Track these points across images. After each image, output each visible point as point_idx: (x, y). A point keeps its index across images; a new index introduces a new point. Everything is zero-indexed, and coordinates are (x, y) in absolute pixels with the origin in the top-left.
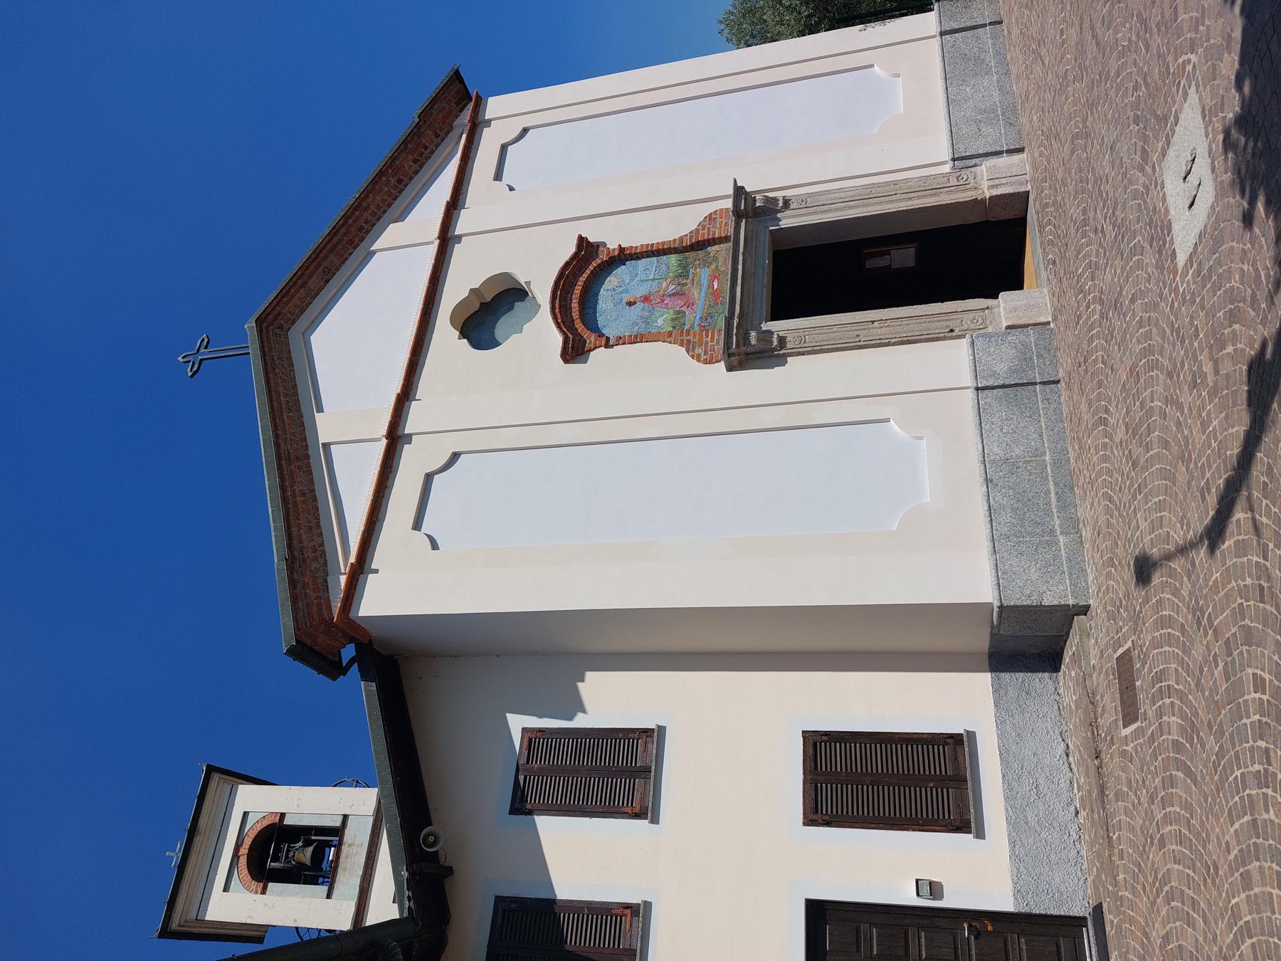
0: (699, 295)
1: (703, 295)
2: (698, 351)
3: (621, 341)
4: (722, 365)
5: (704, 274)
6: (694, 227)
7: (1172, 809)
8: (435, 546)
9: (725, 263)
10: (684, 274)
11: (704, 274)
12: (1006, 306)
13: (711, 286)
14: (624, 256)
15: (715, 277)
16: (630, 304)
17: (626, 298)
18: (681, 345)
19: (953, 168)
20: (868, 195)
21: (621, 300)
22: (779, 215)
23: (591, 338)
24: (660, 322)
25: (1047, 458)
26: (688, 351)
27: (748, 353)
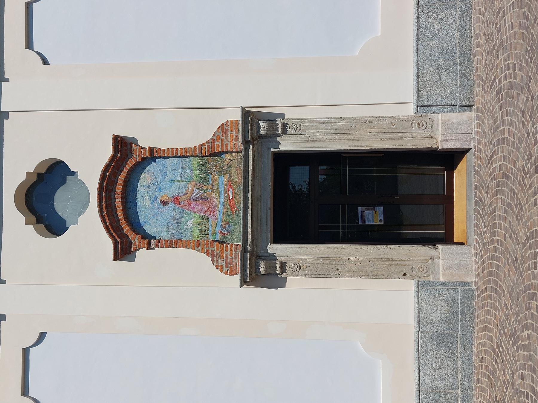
0: (218, 201)
2: (221, 263)
3: (160, 243)
4: (238, 278)
5: (222, 181)
6: (210, 136)
8: (45, 62)
9: (237, 174)
10: (204, 180)
11: (222, 181)
12: (443, 260)
13: (227, 195)
14: (153, 155)
15: (230, 187)
16: (164, 203)
17: (161, 196)
18: (208, 255)
19: (417, 112)
20: (350, 125)
21: (156, 198)
22: (279, 139)
23: (136, 240)
24: (189, 225)
25: (459, 392)
26: (213, 261)
27: (259, 272)
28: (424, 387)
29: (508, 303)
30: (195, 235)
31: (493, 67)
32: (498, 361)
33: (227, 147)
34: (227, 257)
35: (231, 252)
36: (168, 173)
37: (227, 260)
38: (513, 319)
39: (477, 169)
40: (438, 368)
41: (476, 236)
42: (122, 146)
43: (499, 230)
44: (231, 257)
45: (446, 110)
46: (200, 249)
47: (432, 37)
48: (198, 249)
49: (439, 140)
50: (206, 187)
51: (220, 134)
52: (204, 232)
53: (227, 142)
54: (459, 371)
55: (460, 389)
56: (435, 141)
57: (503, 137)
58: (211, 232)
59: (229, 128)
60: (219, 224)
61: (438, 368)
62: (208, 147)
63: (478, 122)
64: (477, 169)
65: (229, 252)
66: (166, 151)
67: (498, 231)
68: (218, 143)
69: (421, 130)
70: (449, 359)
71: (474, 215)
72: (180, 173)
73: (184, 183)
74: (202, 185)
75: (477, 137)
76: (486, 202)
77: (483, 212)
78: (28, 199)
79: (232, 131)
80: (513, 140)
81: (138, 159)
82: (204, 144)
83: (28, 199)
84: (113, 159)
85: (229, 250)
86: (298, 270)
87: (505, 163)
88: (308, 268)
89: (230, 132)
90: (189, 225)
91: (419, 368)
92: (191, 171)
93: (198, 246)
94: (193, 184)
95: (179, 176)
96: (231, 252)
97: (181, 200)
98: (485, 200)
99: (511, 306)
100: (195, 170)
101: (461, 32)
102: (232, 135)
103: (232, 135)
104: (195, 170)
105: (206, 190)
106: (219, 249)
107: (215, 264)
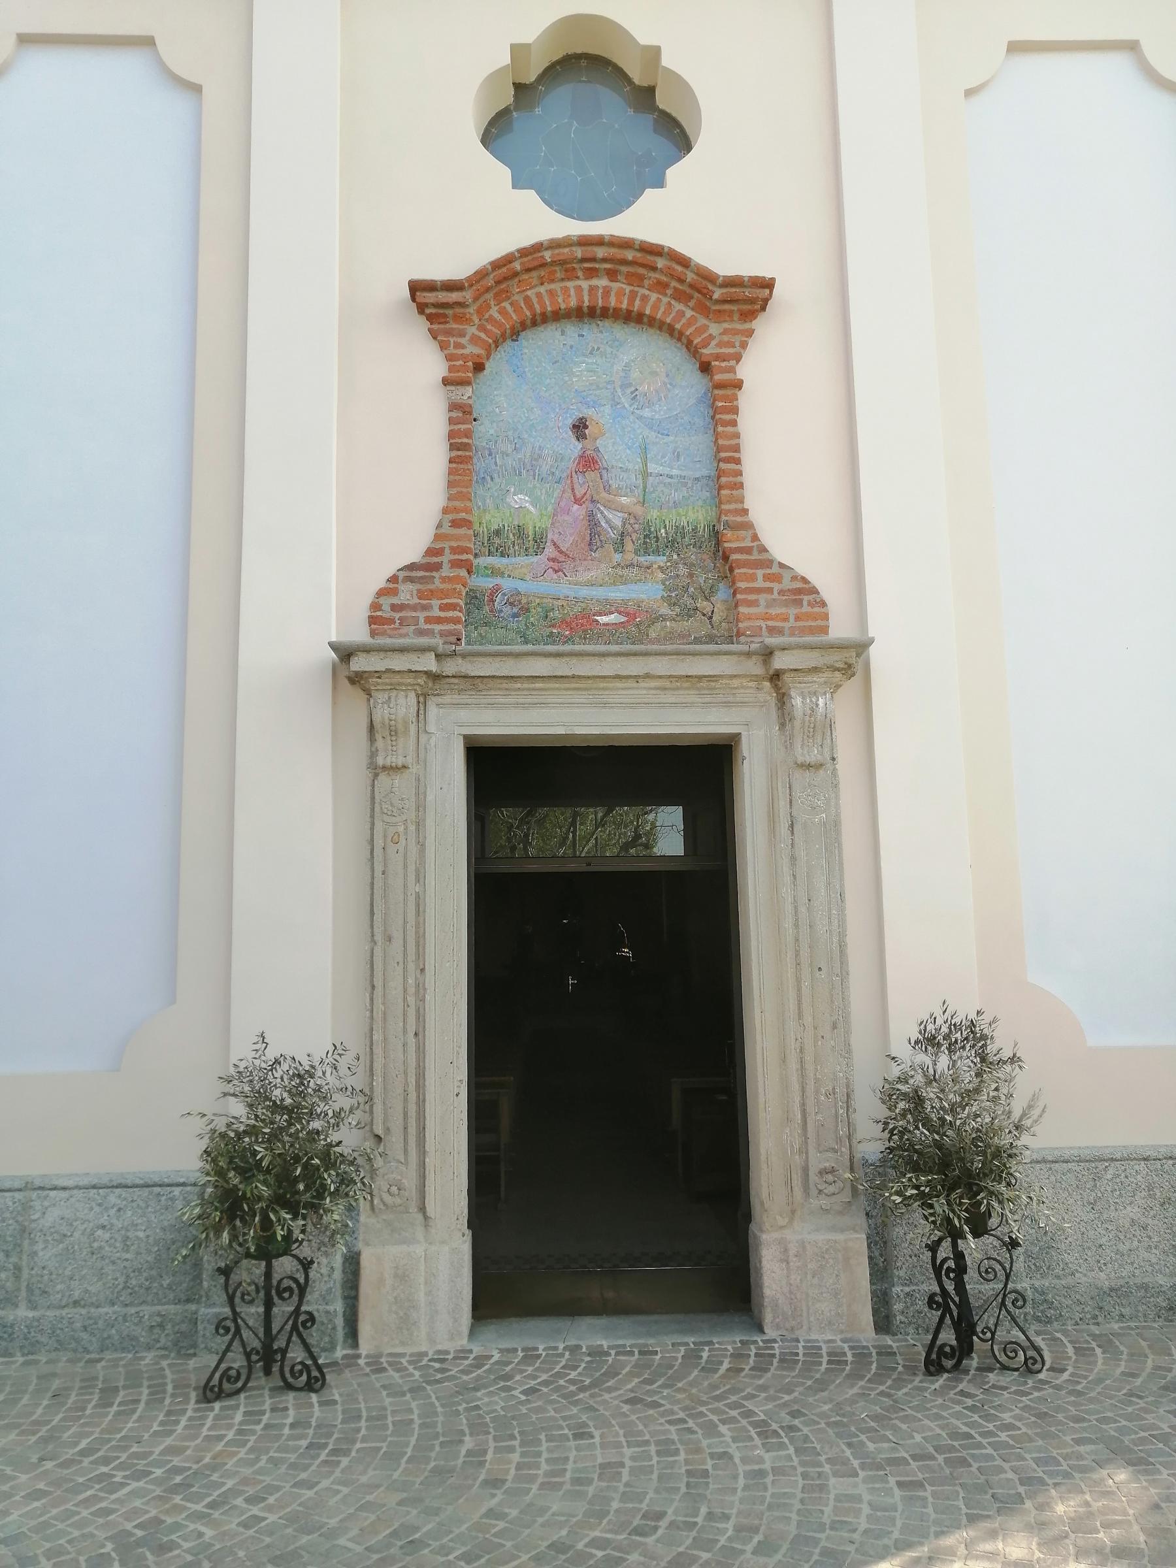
1: (584, 592)
2: (407, 593)
4: (359, 634)
7: (1100, 1362)
8: (969, 93)
10: (650, 542)
13: (608, 607)
14: (721, 394)
16: (580, 428)
17: (601, 417)
18: (430, 552)
24: (519, 500)
26: (411, 567)
28: (37, 1204)
29: (270, 1509)
30: (490, 518)
31: (1042, 1416)
32: (86, 1461)
33: (751, 604)
34: (425, 608)
35: (439, 621)
36: (667, 439)
37: (414, 608)
38: (209, 1533)
39: (705, 1355)
40: (95, 1245)
41: (497, 1356)
42: (749, 298)
43: (516, 1457)
44: (422, 620)
45: (877, 1254)
46: (447, 529)
47: (1093, 1204)
48: (446, 524)
49: (788, 1234)
50: (629, 546)
51: (787, 584)
52: (496, 542)
53: (762, 602)
54: (83, 1311)
55: (31, 1314)
56: (782, 1221)
57: (827, 1468)
58: (496, 561)
59: (806, 609)
60: (522, 586)
61: (95, 1245)
62: (748, 551)
63: (850, 1358)
64: (705, 1355)
65: (436, 613)
66: (730, 429)
67: (511, 1449)
68: (760, 578)
69: (813, 1177)
70: (121, 1280)
71: (561, 1346)
72: (667, 471)
73: (640, 481)
74: (634, 536)
75: (801, 1351)
76: (607, 1396)
77: (572, 1382)
78: (583, 63)
79: (797, 618)
80: (826, 1519)
81: (704, 351)
82: (755, 538)
83: (583, 63)
84: (708, 276)
85: (442, 614)
86: (386, 818)
87: (741, 1482)
88: (392, 848)
89: (792, 611)
90: (519, 500)
91: (94, 1187)
92: (676, 505)
93: (455, 524)
94: (639, 510)
95: (660, 469)
96: (439, 621)
97: (591, 475)
98: (609, 1390)
99: (258, 1519)
100: (679, 514)
101: (1111, 1289)
102: (786, 619)
103: (786, 619)
104: (679, 514)
105: (620, 546)
106: (449, 586)
107: (402, 575)
